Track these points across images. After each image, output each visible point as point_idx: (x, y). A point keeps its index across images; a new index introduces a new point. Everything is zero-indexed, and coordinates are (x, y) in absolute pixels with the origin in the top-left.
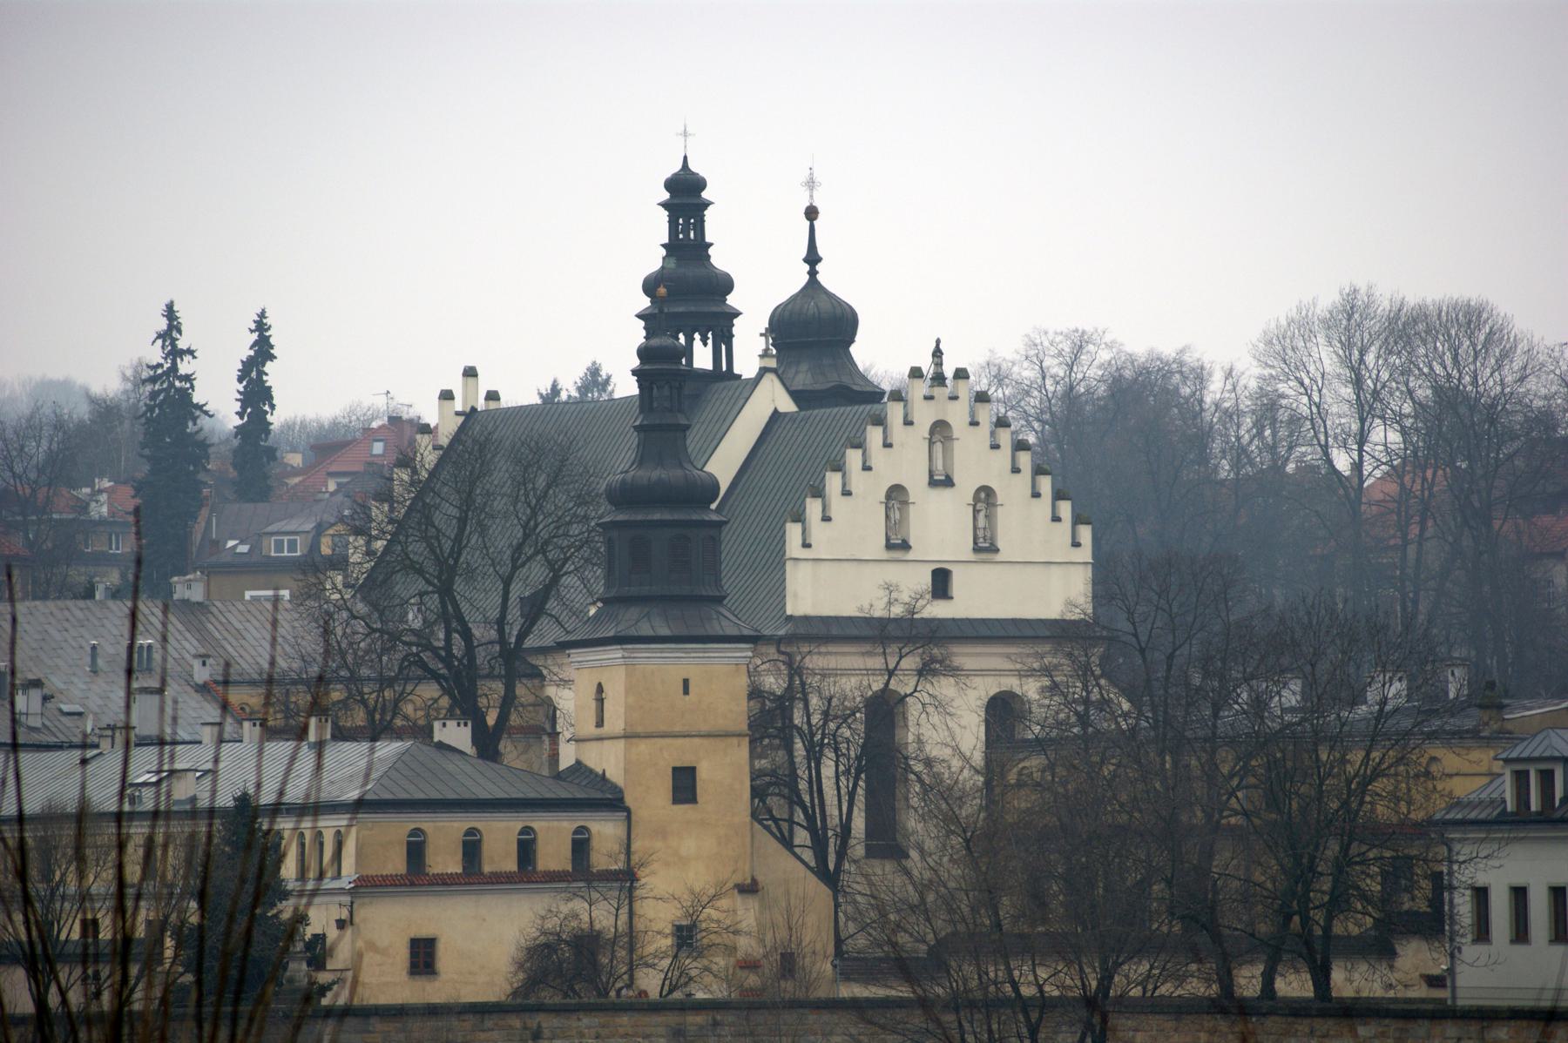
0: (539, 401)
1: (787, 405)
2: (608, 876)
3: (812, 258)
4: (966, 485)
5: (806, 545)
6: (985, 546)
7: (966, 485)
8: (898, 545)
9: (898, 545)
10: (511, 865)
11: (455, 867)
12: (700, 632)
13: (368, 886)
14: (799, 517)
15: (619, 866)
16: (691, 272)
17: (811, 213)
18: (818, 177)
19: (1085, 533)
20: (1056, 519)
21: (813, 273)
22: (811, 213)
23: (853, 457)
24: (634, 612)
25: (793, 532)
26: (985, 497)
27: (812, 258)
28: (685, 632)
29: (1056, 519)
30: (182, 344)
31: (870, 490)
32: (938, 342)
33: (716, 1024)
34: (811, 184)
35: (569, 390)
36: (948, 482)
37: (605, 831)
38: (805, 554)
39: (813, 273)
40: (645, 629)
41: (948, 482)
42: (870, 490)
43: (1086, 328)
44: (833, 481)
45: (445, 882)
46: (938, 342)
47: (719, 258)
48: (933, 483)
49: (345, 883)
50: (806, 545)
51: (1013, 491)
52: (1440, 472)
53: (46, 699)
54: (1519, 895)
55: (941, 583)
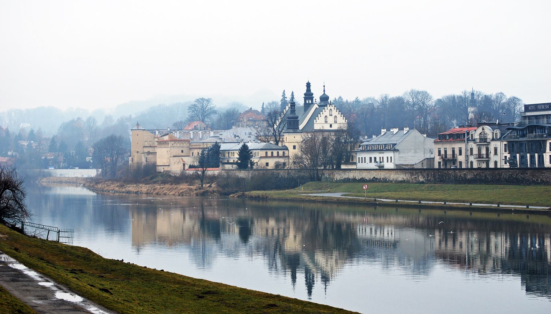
0: (260, 110)
1: (318, 107)
2: (287, 156)
3: (324, 91)
4: (334, 115)
5: (316, 122)
6: (336, 122)
7: (334, 115)
8: (326, 122)
9: (326, 122)
10: (276, 155)
11: (276, 155)
12: (296, 132)
13: (261, 157)
14: (316, 119)
15: (288, 155)
16: (309, 93)
17: (324, 86)
18: (325, 82)
19: (346, 121)
20: (343, 119)
21: (324, 92)
22: (324, 86)
23: (321, 113)
24: (289, 130)
25: (315, 120)
26: (336, 117)
27: (324, 91)
28: (294, 132)
29: (343, 119)
30: (285, 96)
31: (323, 116)
32: (308, 85)
33: (292, 171)
34: (324, 83)
35: (337, 99)
36: (332, 115)
37: (286, 152)
38: (316, 123)
39: (324, 92)
40: (290, 132)
41: (332, 115)
42: (323, 116)
43: (343, 99)
44: (319, 115)
45: (269, 157)
46: (308, 85)
47: (312, 91)
48: (330, 115)
49: (259, 157)
50: (316, 122)
51: (339, 116)
52: (464, 106)
53: (239, 138)
54: (362, 158)
55: (331, 126)
